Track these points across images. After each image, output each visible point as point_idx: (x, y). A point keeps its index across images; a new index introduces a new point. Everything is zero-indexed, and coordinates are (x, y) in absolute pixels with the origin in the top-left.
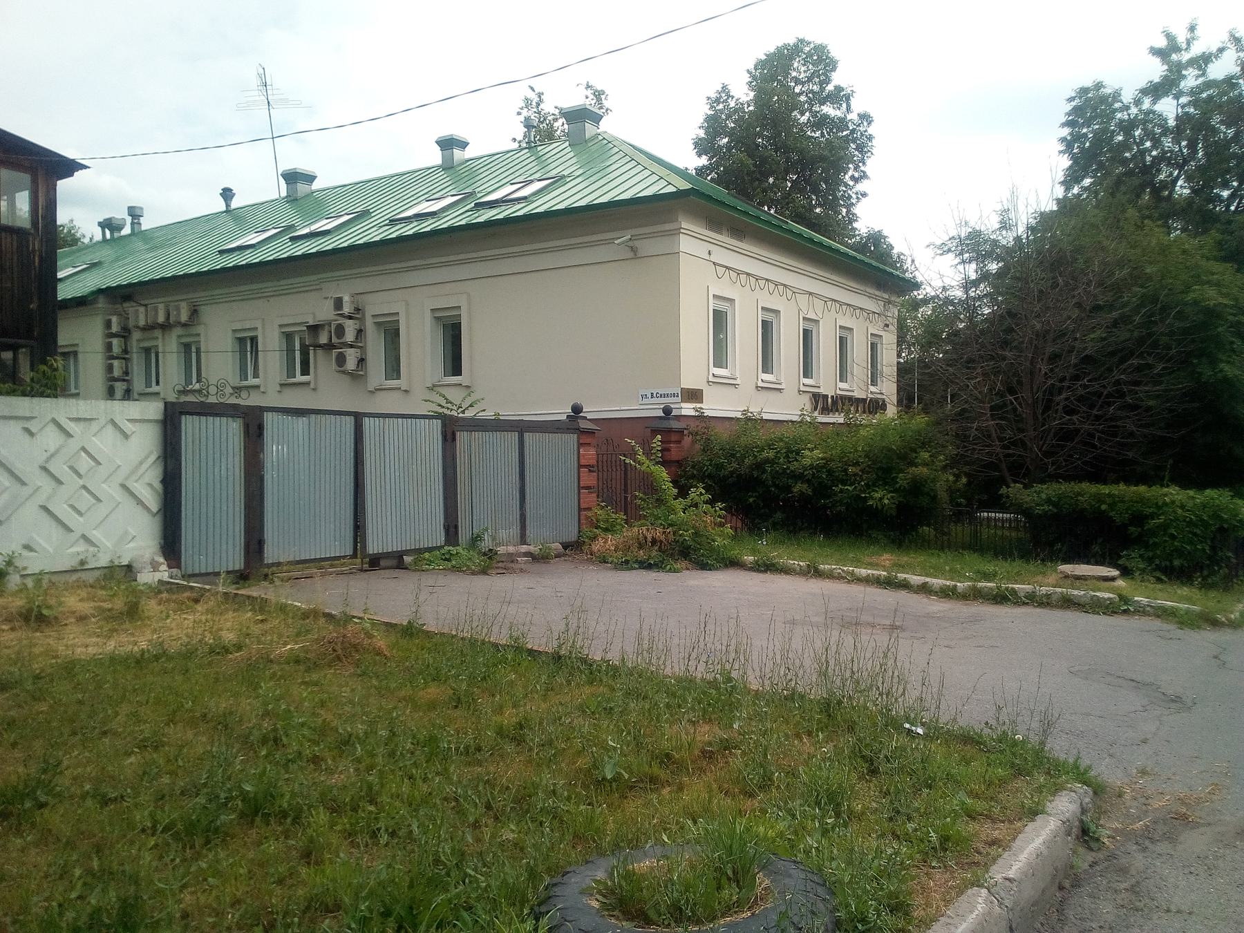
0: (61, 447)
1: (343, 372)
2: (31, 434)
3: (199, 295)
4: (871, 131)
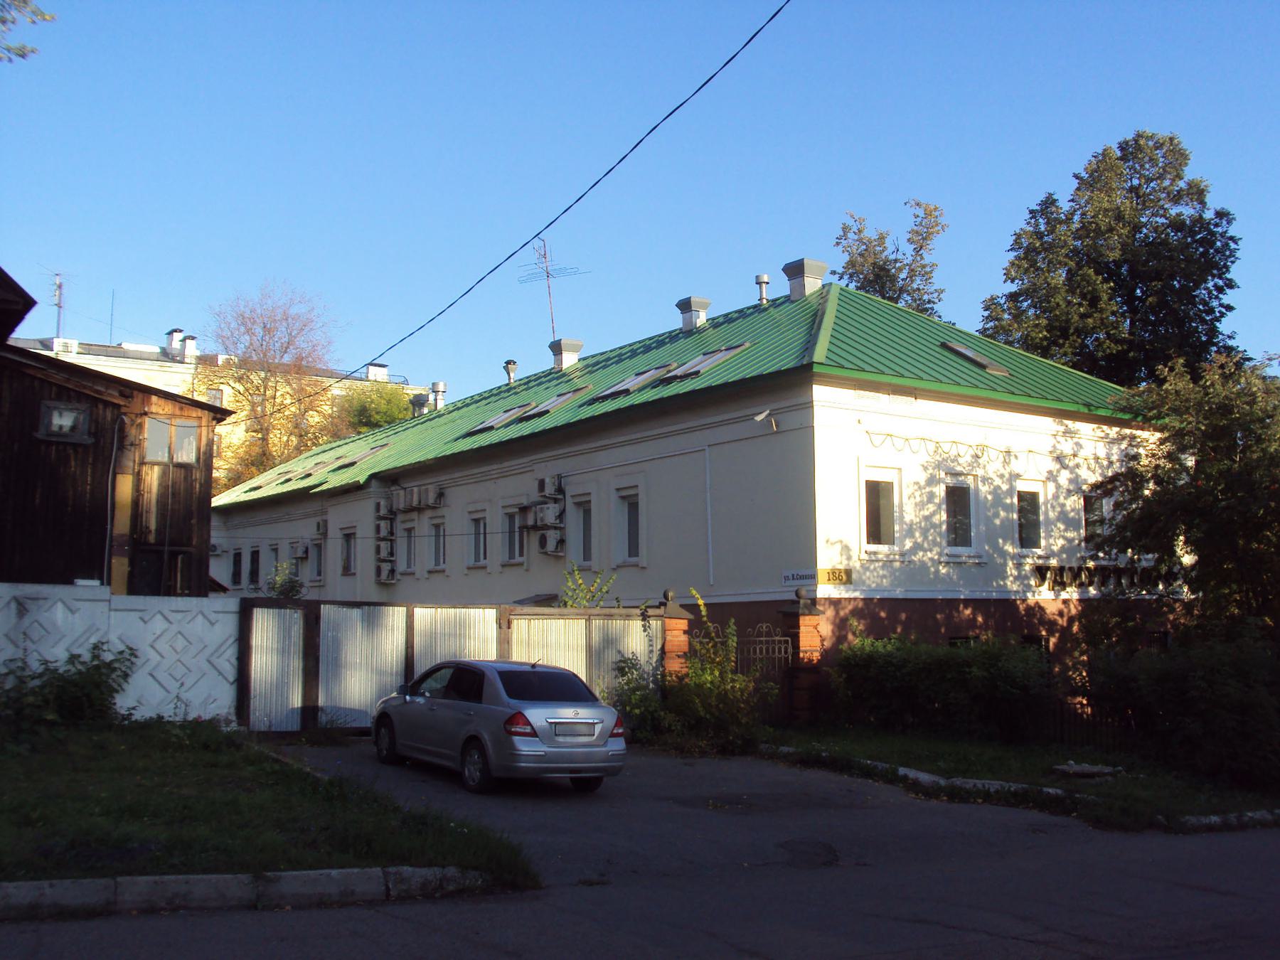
0: (166, 630)
1: (546, 553)
2: (145, 622)
3: (443, 478)
4: (1232, 232)
